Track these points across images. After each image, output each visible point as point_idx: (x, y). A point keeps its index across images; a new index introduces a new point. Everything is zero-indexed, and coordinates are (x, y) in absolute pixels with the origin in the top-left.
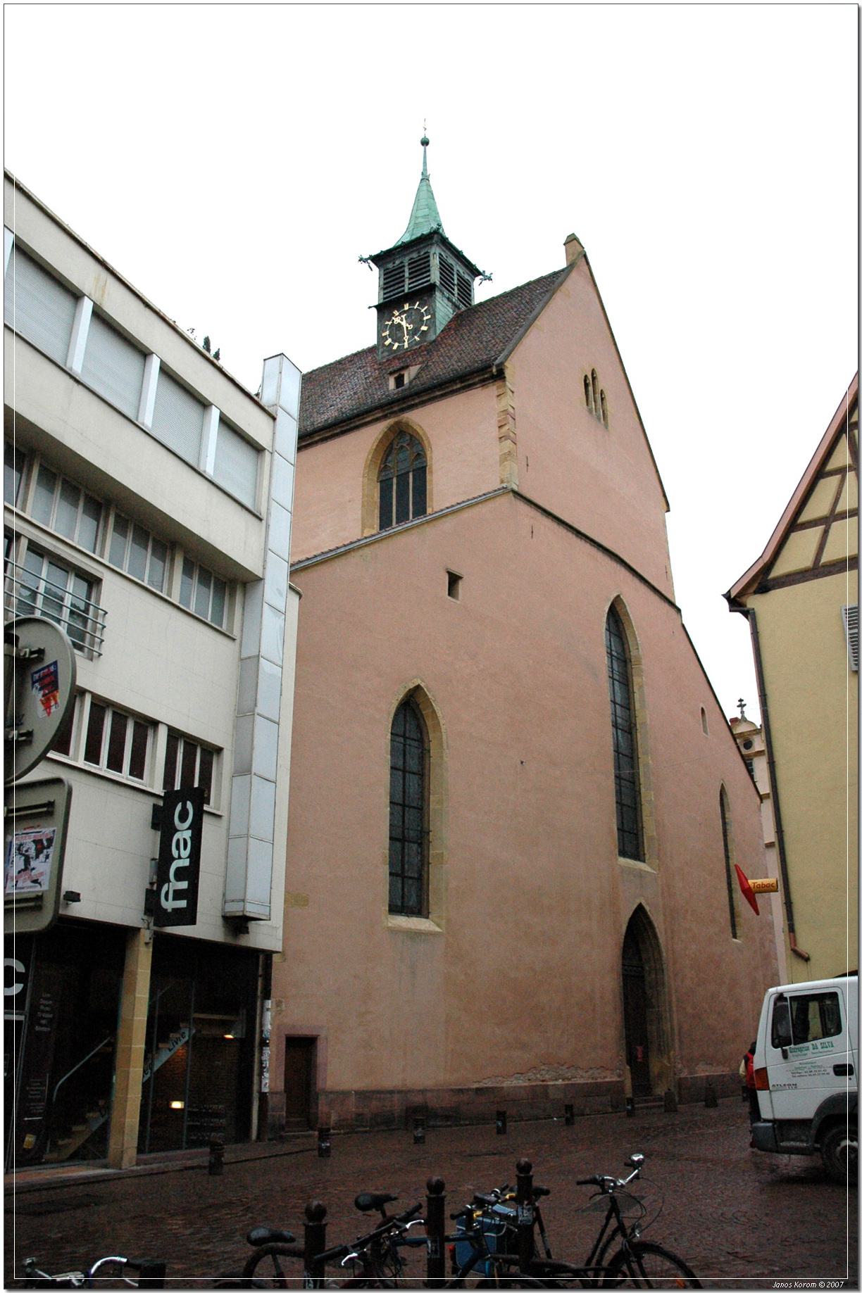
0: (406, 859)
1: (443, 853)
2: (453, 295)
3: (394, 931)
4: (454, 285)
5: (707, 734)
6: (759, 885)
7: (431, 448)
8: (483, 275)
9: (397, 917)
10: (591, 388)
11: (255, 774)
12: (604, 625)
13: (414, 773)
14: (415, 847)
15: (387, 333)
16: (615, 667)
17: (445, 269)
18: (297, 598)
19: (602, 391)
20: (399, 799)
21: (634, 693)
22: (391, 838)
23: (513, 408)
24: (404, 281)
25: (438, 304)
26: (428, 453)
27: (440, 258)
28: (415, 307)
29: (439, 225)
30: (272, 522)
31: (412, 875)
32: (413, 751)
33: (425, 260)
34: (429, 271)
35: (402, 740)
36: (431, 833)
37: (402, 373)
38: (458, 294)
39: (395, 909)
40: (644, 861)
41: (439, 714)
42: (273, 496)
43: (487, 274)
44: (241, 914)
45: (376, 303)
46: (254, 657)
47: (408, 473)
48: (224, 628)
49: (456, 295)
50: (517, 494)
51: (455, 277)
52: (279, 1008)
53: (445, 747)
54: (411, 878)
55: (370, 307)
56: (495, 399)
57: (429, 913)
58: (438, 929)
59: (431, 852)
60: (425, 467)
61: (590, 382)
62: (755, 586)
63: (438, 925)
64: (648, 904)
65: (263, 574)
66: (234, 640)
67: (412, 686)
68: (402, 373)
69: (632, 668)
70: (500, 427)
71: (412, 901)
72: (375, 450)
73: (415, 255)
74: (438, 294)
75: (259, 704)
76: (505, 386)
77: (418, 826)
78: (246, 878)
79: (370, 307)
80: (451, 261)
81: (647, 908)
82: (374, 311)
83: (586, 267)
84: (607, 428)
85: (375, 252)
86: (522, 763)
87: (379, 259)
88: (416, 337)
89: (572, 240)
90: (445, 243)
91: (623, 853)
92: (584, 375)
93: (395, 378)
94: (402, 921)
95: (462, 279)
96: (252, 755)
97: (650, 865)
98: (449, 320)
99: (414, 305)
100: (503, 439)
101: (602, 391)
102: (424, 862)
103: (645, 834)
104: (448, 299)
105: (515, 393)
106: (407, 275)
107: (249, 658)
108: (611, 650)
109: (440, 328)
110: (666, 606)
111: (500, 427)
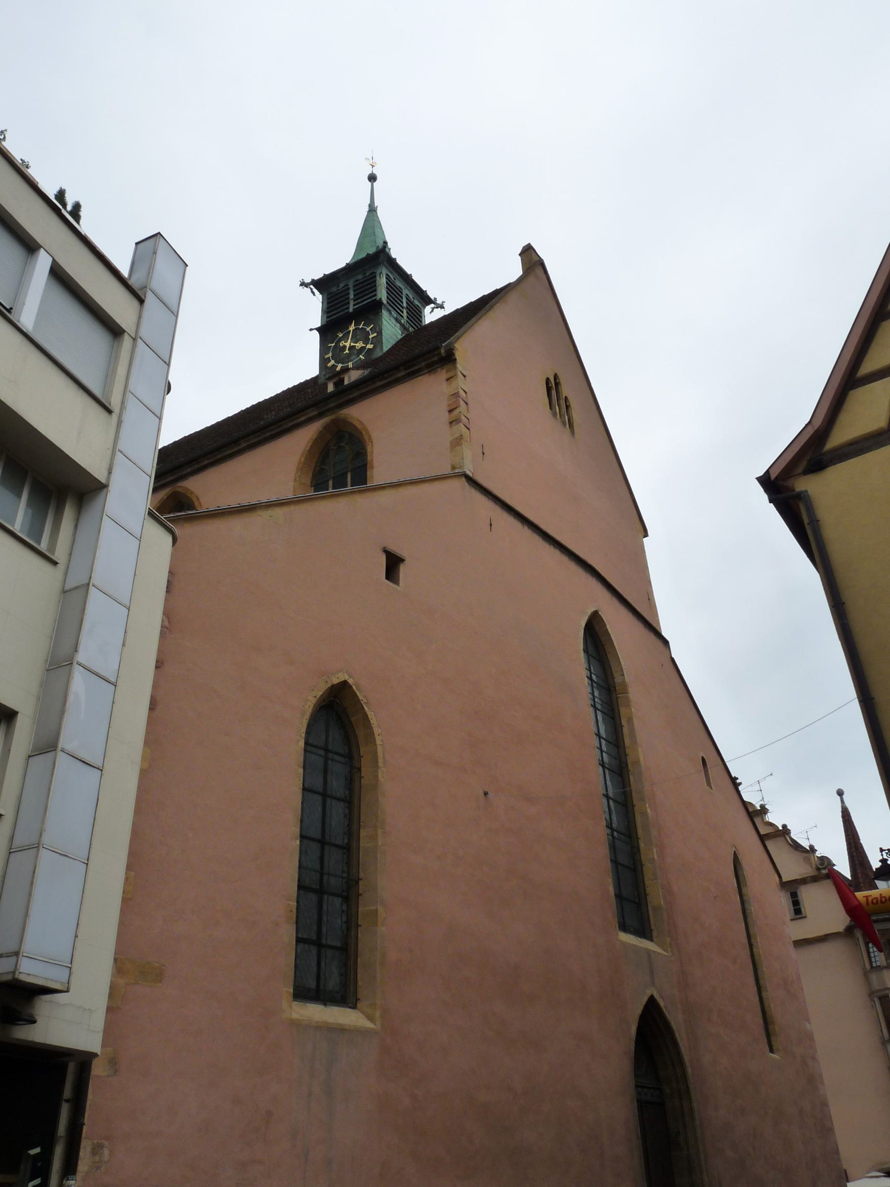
0: (324, 918)
1: (377, 909)
2: (402, 317)
3: (296, 1024)
4: (403, 307)
5: (711, 789)
6: (876, 898)
7: (372, 442)
8: (434, 304)
9: (308, 1005)
10: (554, 393)
11: (63, 751)
12: (581, 646)
13: (339, 799)
14: (338, 901)
15: (330, 355)
16: (596, 693)
17: (392, 288)
18: (169, 539)
19: (566, 397)
20: (315, 833)
21: (622, 726)
22: (301, 887)
23: (466, 392)
24: (348, 303)
25: (384, 322)
26: (369, 449)
27: (386, 278)
28: (360, 327)
29: (385, 243)
30: (126, 418)
31: (334, 944)
32: (338, 768)
33: (372, 280)
34: (375, 290)
35: (322, 752)
36: (361, 883)
37: (342, 377)
38: (407, 317)
39: (302, 994)
40: (652, 941)
41: (374, 721)
42: (131, 386)
43: (439, 302)
44: (9, 977)
45: (319, 325)
46: (83, 585)
47: (346, 473)
48: (43, 546)
49: (405, 318)
50: (472, 481)
51: (404, 300)
52: (97, 1158)
53: (381, 764)
54: (331, 947)
55: (311, 330)
56: (445, 383)
57: (357, 1000)
58: (369, 1025)
59: (360, 909)
60: (366, 464)
61: (553, 387)
62: (801, 468)
63: (371, 1018)
64: (662, 997)
65: (108, 478)
66: (55, 563)
67: (336, 681)
68: (342, 377)
69: (617, 698)
70: (450, 411)
71: (332, 982)
72: (309, 451)
73: (360, 277)
74: (385, 313)
75: (81, 648)
76: (455, 368)
77: (344, 872)
78: (26, 915)
79: (311, 330)
80: (399, 283)
81: (662, 1003)
82: (316, 335)
83: (544, 276)
84: (573, 436)
85: (318, 276)
86: (486, 794)
87: (322, 284)
88: (361, 356)
89: (528, 253)
90: (392, 264)
91: (624, 928)
92: (545, 378)
93: (334, 383)
94: (315, 1012)
95: (412, 303)
96: (60, 724)
97: (661, 945)
98: (397, 340)
99: (360, 325)
100: (454, 423)
101: (566, 397)
102: (351, 925)
103: (649, 904)
104: (396, 319)
105: (467, 378)
106: (352, 296)
107: (76, 588)
108: (591, 673)
109: (386, 347)
110: (652, 636)
111: (450, 411)
